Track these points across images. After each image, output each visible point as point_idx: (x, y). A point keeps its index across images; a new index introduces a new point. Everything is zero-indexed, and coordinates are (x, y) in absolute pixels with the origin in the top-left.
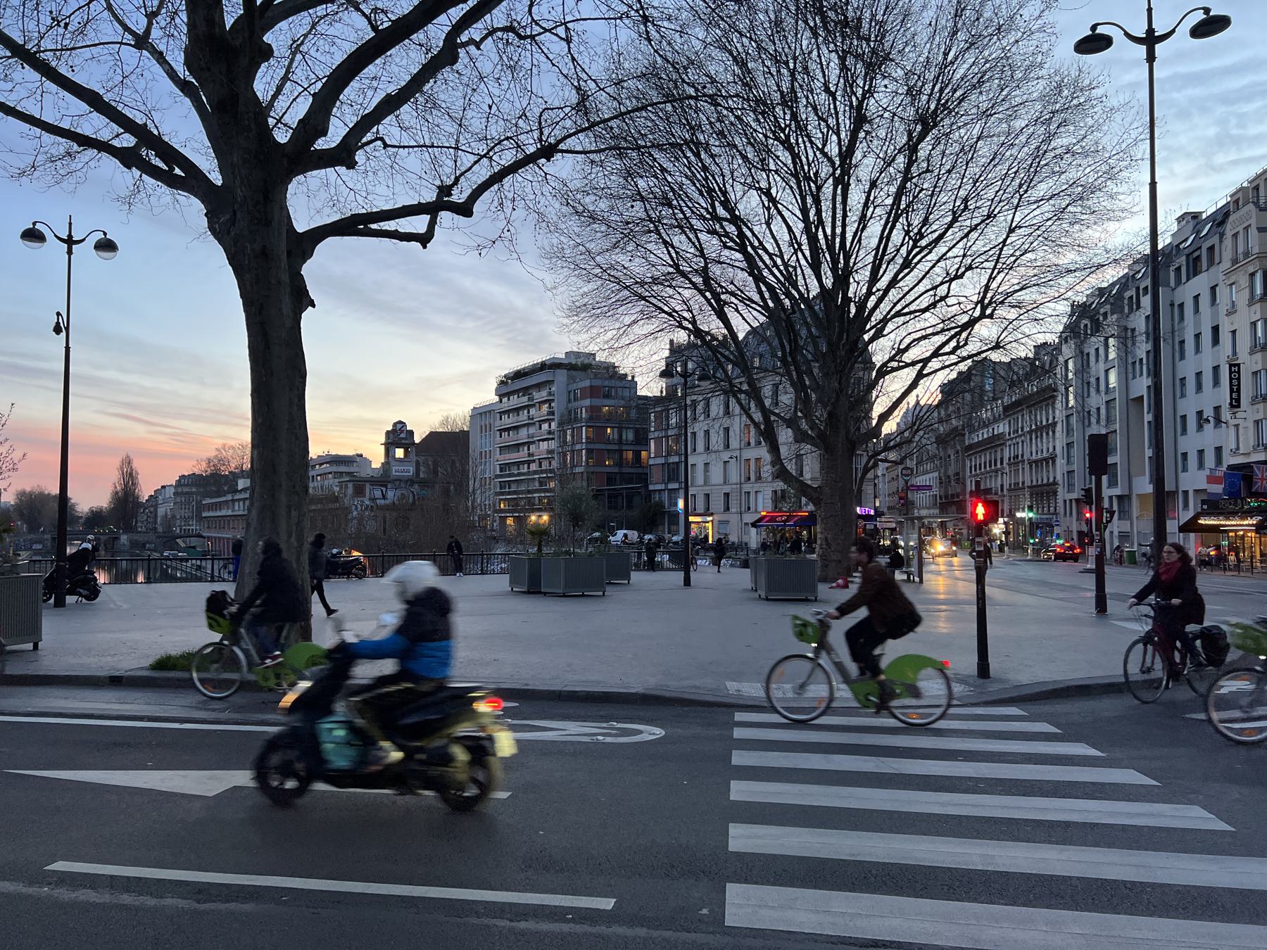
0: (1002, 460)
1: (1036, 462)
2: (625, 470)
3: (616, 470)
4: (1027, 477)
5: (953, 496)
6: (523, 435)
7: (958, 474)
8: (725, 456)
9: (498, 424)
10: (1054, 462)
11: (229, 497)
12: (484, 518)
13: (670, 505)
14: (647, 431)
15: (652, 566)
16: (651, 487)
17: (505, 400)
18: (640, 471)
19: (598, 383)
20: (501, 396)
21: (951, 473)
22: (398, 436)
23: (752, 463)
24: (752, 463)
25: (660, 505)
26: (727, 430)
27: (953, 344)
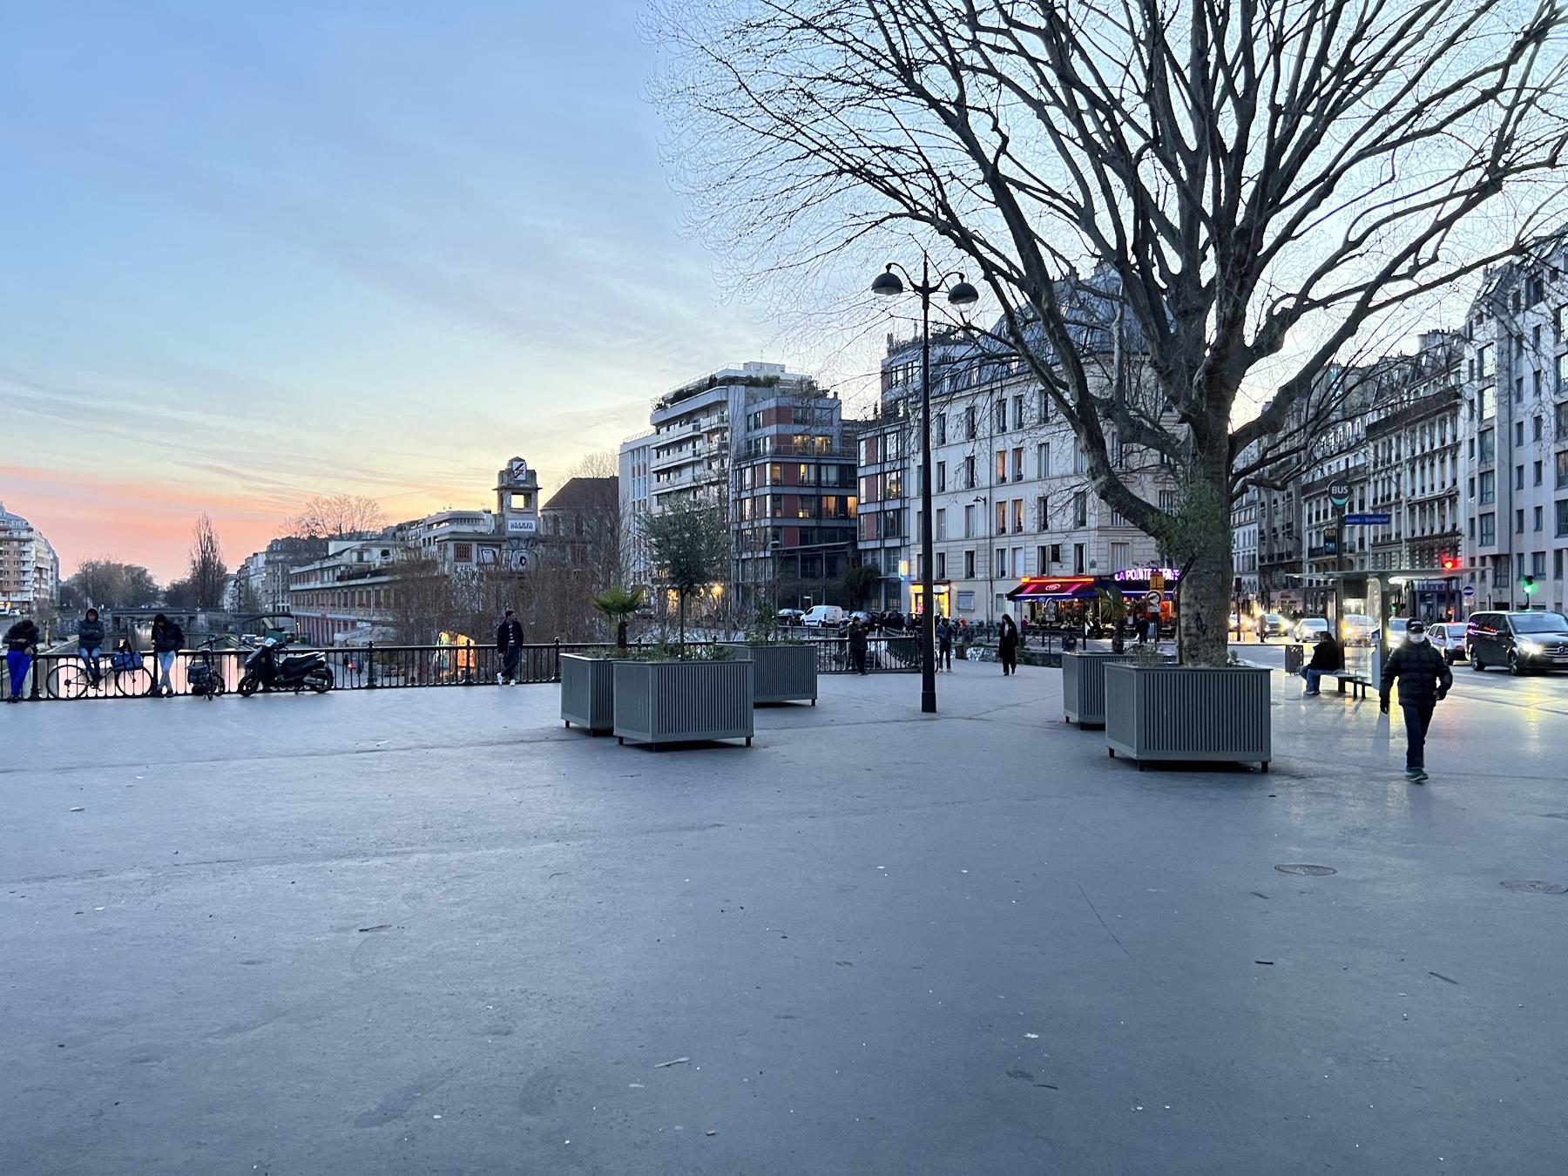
0: (1318, 513)
1: (1422, 504)
2: (825, 523)
3: (813, 523)
4: (1403, 525)
5: (1281, 556)
6: (686, 479)
7: (1289, 525)
8: (969, 498)
9: (656, 464)
10: (1453, 501)
11: (317, 565)
12: (637, 590)
13: (888, 570)
14: (854, 468)
15: (861, 663)
16: (861, 546)
17: (664, 430)
18: (845, 524)
19: (784, 402)
20: (659, 425)
21: (1277, 524)
22: (518, 480)
23: (1009, 508)
24: (1009, 508)
25: (875, 570)
26: (971, 461)
27: (1409, 262)
